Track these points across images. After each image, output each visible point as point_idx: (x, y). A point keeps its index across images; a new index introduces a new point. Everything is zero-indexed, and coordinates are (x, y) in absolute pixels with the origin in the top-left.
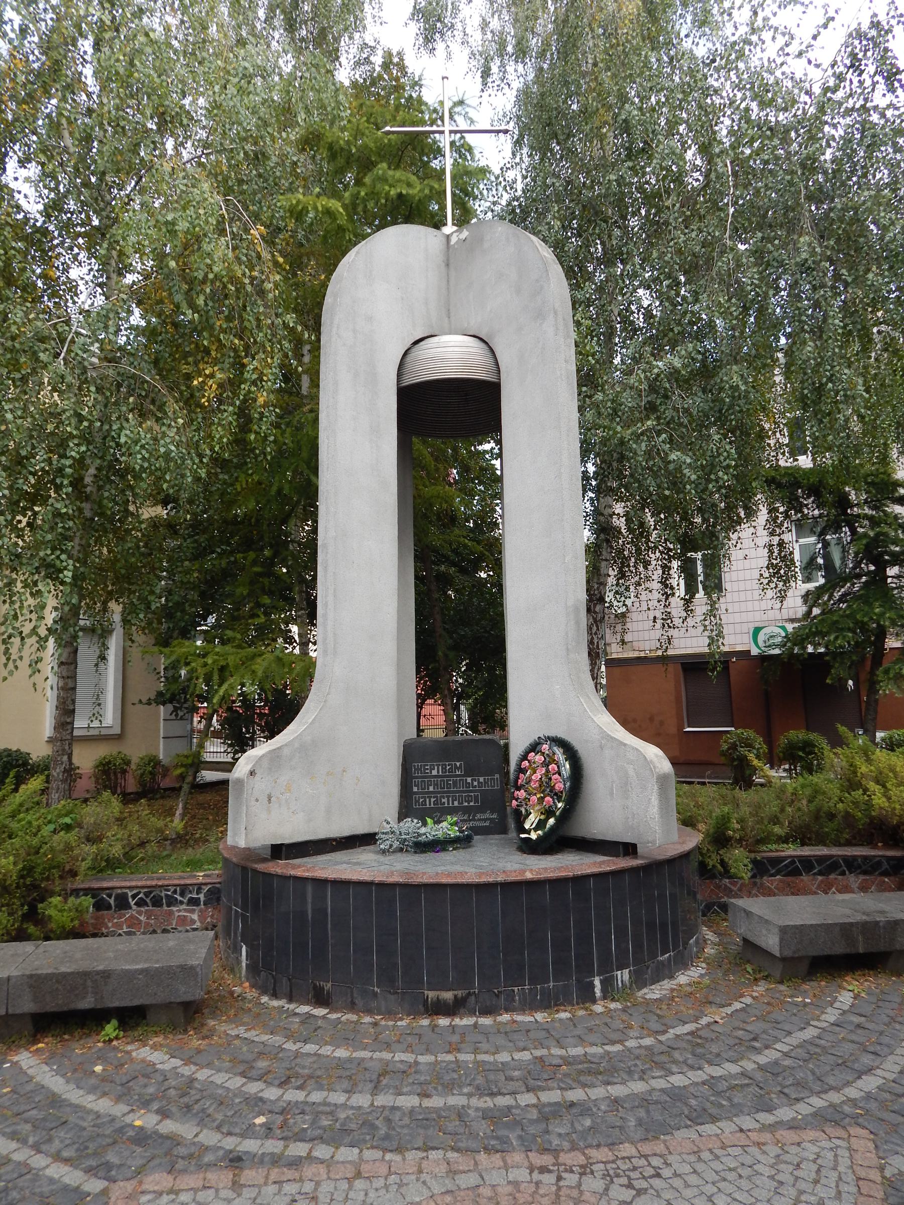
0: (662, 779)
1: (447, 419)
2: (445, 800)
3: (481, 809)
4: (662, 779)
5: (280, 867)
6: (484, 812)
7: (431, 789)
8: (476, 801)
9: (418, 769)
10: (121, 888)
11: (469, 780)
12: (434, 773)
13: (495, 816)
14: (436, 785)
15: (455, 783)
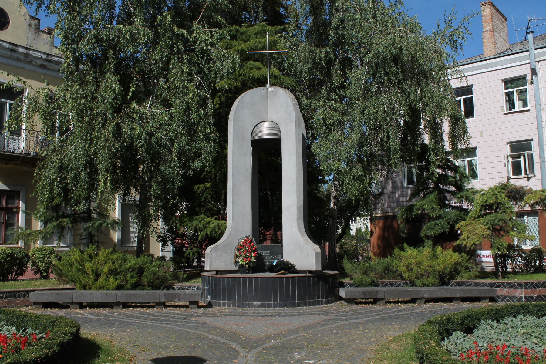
1: (267, 153)
5: (219, 276)
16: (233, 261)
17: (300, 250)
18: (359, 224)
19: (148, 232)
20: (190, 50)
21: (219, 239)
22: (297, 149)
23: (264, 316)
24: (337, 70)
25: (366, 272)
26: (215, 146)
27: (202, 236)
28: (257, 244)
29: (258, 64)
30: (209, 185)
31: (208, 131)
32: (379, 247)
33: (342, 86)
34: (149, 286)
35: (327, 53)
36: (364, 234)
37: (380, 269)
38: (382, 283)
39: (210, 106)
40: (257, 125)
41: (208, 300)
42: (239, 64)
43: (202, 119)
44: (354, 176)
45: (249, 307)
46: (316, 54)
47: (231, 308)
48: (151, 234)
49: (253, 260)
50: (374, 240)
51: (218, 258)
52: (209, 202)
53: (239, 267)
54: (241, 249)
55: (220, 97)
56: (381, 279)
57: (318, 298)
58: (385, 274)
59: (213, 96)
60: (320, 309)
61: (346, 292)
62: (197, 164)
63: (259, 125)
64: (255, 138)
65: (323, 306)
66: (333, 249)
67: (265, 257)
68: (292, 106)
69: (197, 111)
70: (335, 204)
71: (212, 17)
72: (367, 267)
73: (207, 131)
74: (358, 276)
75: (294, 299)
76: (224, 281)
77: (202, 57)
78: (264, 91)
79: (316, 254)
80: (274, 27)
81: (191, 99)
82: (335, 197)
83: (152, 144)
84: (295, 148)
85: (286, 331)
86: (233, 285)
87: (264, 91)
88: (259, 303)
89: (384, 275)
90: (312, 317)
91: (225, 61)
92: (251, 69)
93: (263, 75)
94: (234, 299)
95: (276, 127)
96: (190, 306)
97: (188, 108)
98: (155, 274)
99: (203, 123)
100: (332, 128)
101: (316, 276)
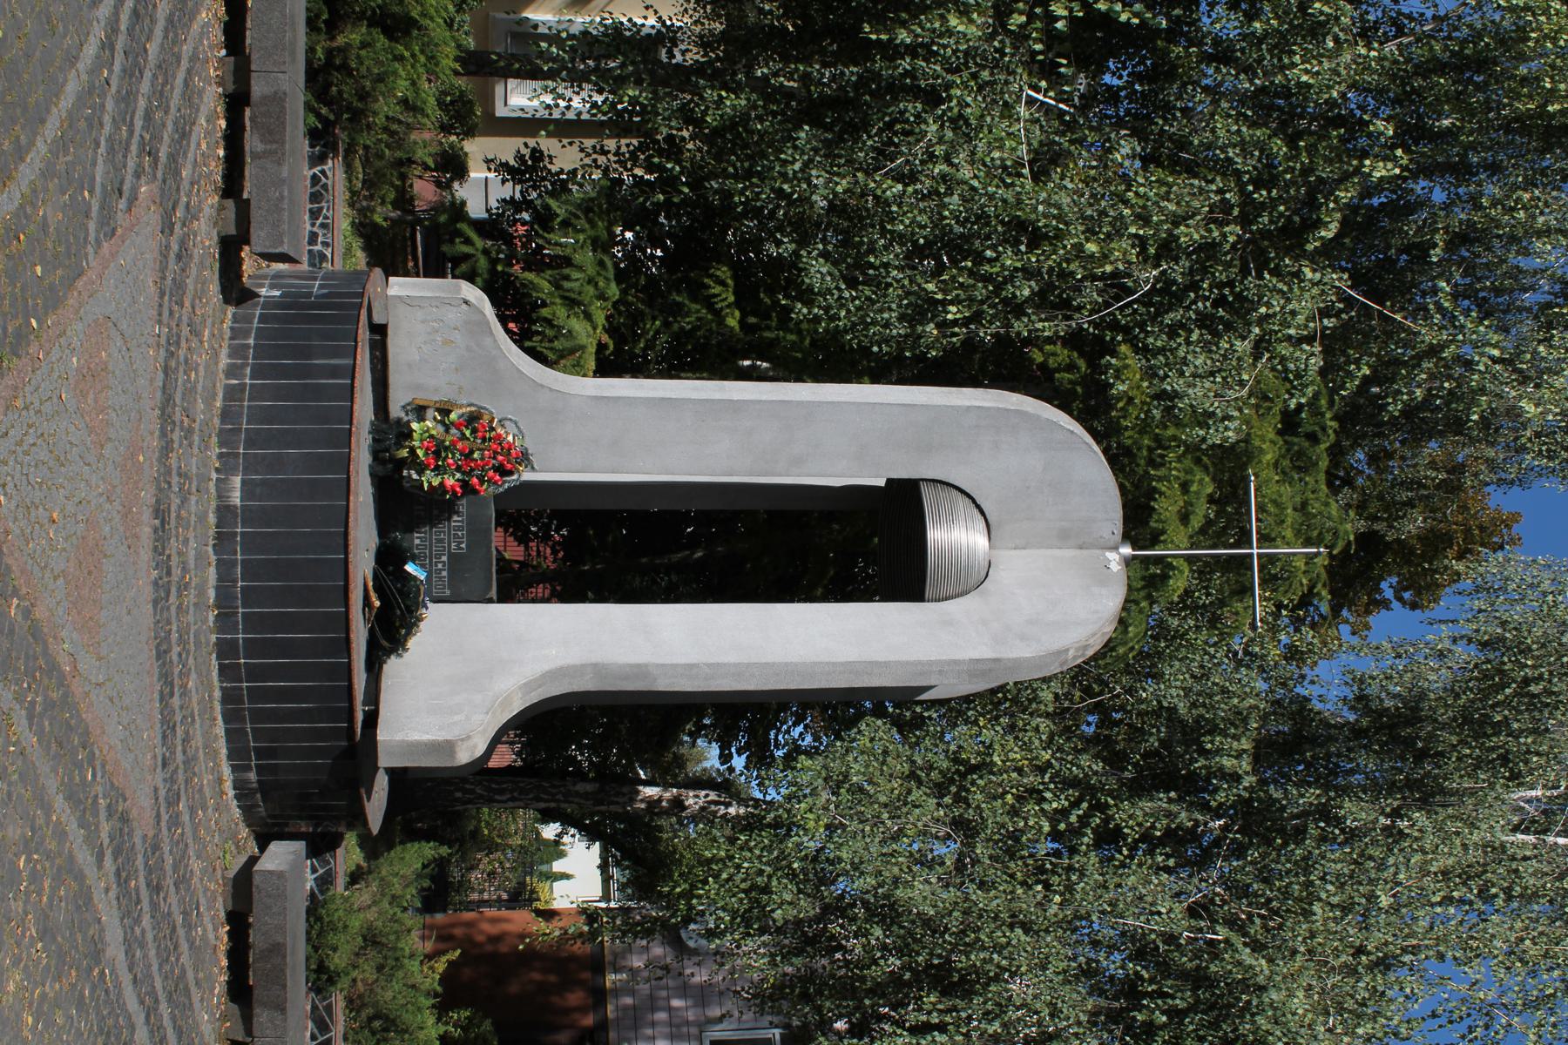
1: (866, 543)
5: (364, 334)
11: (444, 558)
15: (441, 541)
16: (423, 397)
17: (469, 673)
18: (579, 875)
19: (551, 75)
20: (1255, 256)
21: (520, 339)
22: (886, 664)
23: (160, 513)
24: (1170, 815)
25: (375, 943)
26: (887, 341)
27: (536, 288)
28: (497, 498)
29: (1202, 511)
30: (732, 322)
31: (953, 312)
32: (496, 939)
33: (1109, 837)
34: (329, 53)
35: (1235, 778)
36: (544, 868)
37: (390, 995)
38: (329, 1008)
39: (1046, 328)
40: (978, 507)
41: (263, 291)
42: (1204, 440)
43: (996, 293)
44: (766, 890)
45: (221, 456)
46: (1234, 737)
47: (222, 382)
48: (545, 89)
49: (430, 479)
50: (521, 920)
51: (437, 332)
52: (666, 324)
53: (399, 420)
54: (474, 431)
55: (1071, 367)
56: (350, 1001)
57: (260, 753)
58: (370, 1019)
59: (1074, 340)
60: (203, 764)
61: (280, 875)
62: (818, 272)
63: (976, 511)
64: (927, 494)
65: (227, 772)
66: (481, 796)
67: (440, 532)
68: (1056, 644)
69: (1028, 273)
70: (653, 804)
71: (1362, 348)
72: (395, 949)
73: (953, 309)
74: (360, 907)
75: (253, 648)
76: (336, 353)
77: (1220, 302)
78: (1106, 534)
79: (448, 747)
80: (1324, 576)
81: (1079, 248)
82: (678, 804)
83: (895, 100)
84: (892, 658)
85: (27, 613)
86: (319, 392)
87: (1106, 534)
88: (236, 498)
89: (364, 1015)
90: (151, 734)
91: (1215, 388)
92: (1185, 487)
93: (1163, 532)
94: (257, 393)
95: (972, 582)
96: (230, 203)
97: (1037, 239)
98: (380, 79)
99: (980, 292)
100: (947, 800)
101: (357, 751)
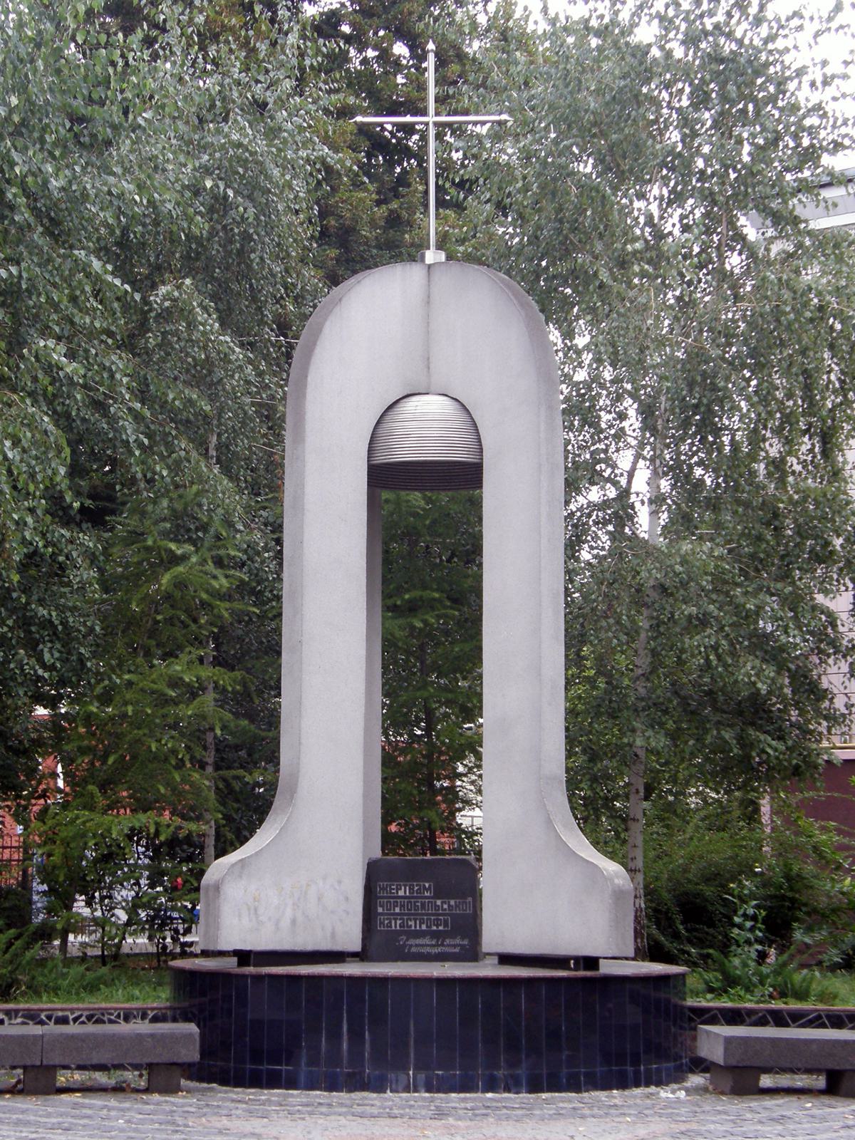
0: (618, 894)
1: (426, 525)
2: (412, 923)
3: (451, 934)
4: (618, 894)
6: (454, 937)
7: (397, 910)
8: (446, 925)
9: (383, 889)
10: (62, 1010)
11: (439, 902)
12: (401, 893)
13: (466, 942)
14: (402, 906)
64: (381, 459)
